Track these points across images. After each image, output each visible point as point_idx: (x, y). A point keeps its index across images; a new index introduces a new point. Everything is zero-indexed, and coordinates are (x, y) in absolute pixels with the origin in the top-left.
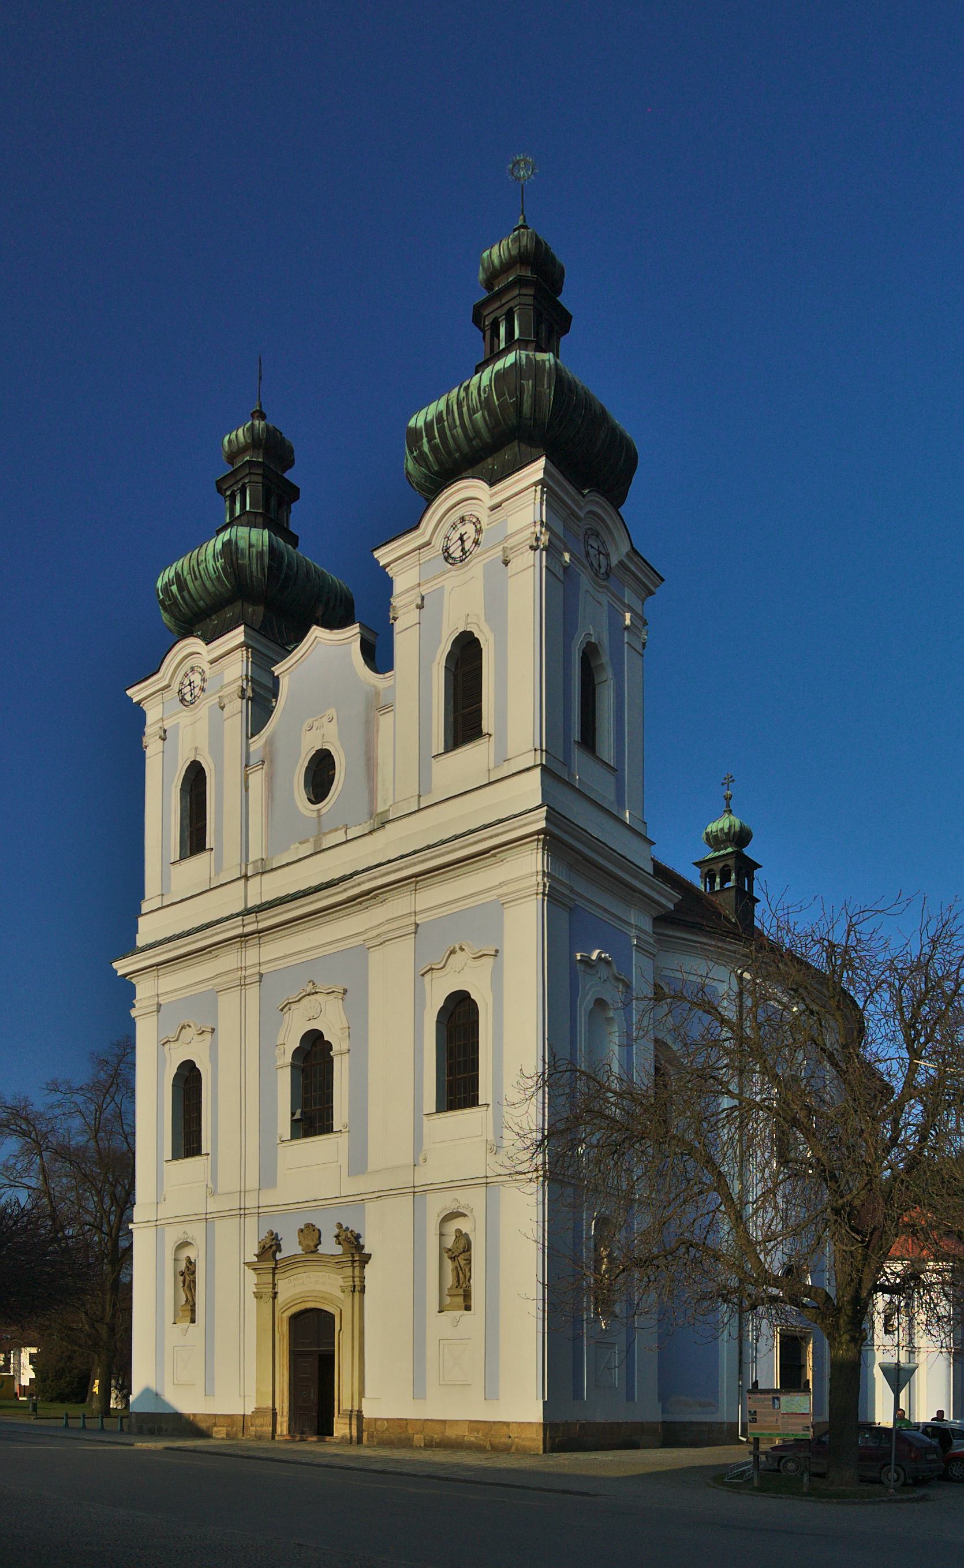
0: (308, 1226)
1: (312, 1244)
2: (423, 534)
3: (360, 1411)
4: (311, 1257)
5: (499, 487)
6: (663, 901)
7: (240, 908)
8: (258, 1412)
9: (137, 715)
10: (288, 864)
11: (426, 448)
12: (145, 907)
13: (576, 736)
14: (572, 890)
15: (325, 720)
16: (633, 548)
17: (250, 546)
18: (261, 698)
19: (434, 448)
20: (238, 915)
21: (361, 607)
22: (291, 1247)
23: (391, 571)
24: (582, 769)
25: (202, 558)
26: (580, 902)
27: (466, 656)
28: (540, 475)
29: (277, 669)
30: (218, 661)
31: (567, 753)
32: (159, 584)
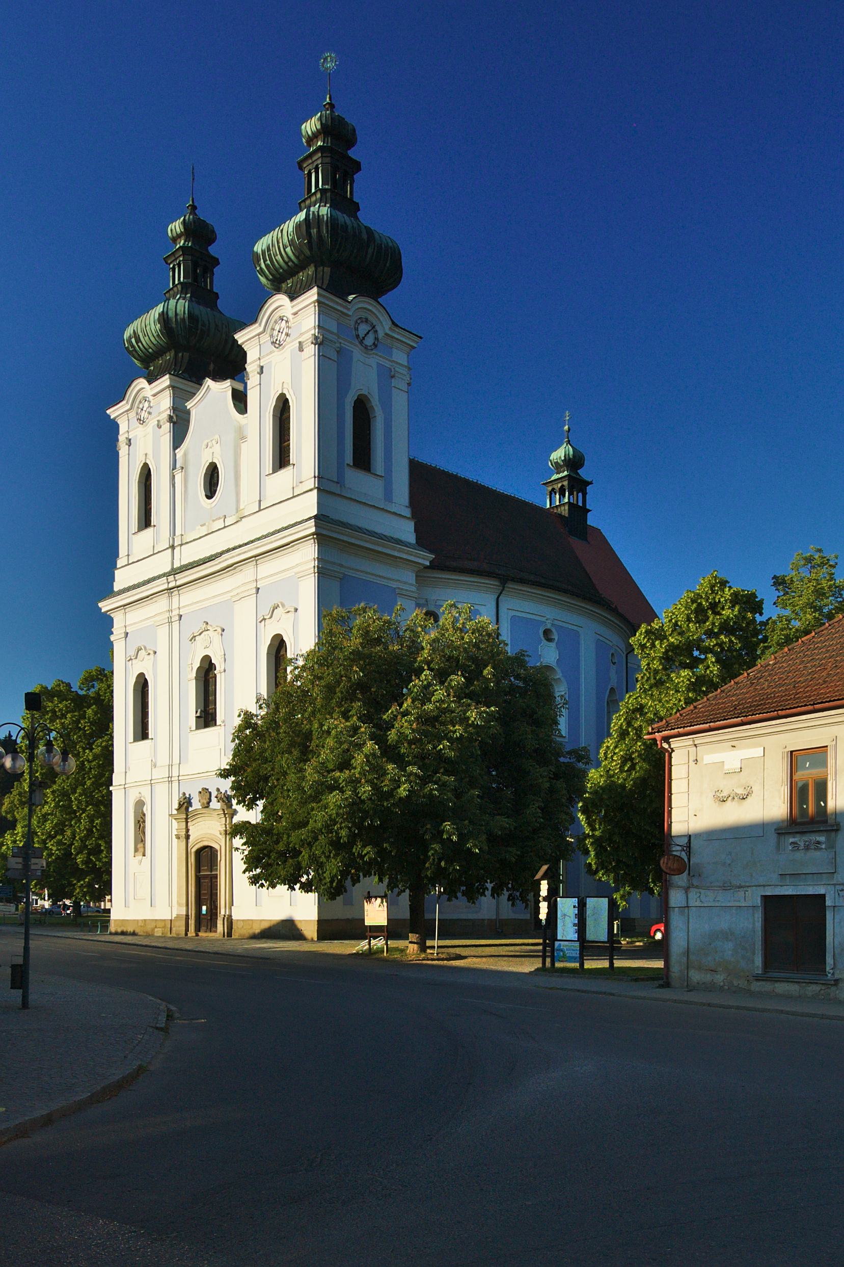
0: (203, 789)
1: (205, 802)
2: (260, 325)
3: (230, 916)
4: (204, 811)
5: (295, 302)
6: (420, 561)
7: (168, 569)
8: (178, 916)
9: (114, 427)
10: (194, 540)
11: (263, 266)
12: (120, 563)
13: (349, 458)
14: (341, 566)
15: (214, 442)
16: (393, 323)
17: (176, 314)
18: (180, 423)
19: (267, 266)
20: (164, 575)
21: (231, 365)
22: (196, 805)
23: (245, 347)
24: (356, 480)
25: (147, 322)
26: (350, 573)
27: (283, 408)
28: (315, 297)
29: (189, 405)
30: (153, 395)
31: (341, 474)
32: (126, 337)
